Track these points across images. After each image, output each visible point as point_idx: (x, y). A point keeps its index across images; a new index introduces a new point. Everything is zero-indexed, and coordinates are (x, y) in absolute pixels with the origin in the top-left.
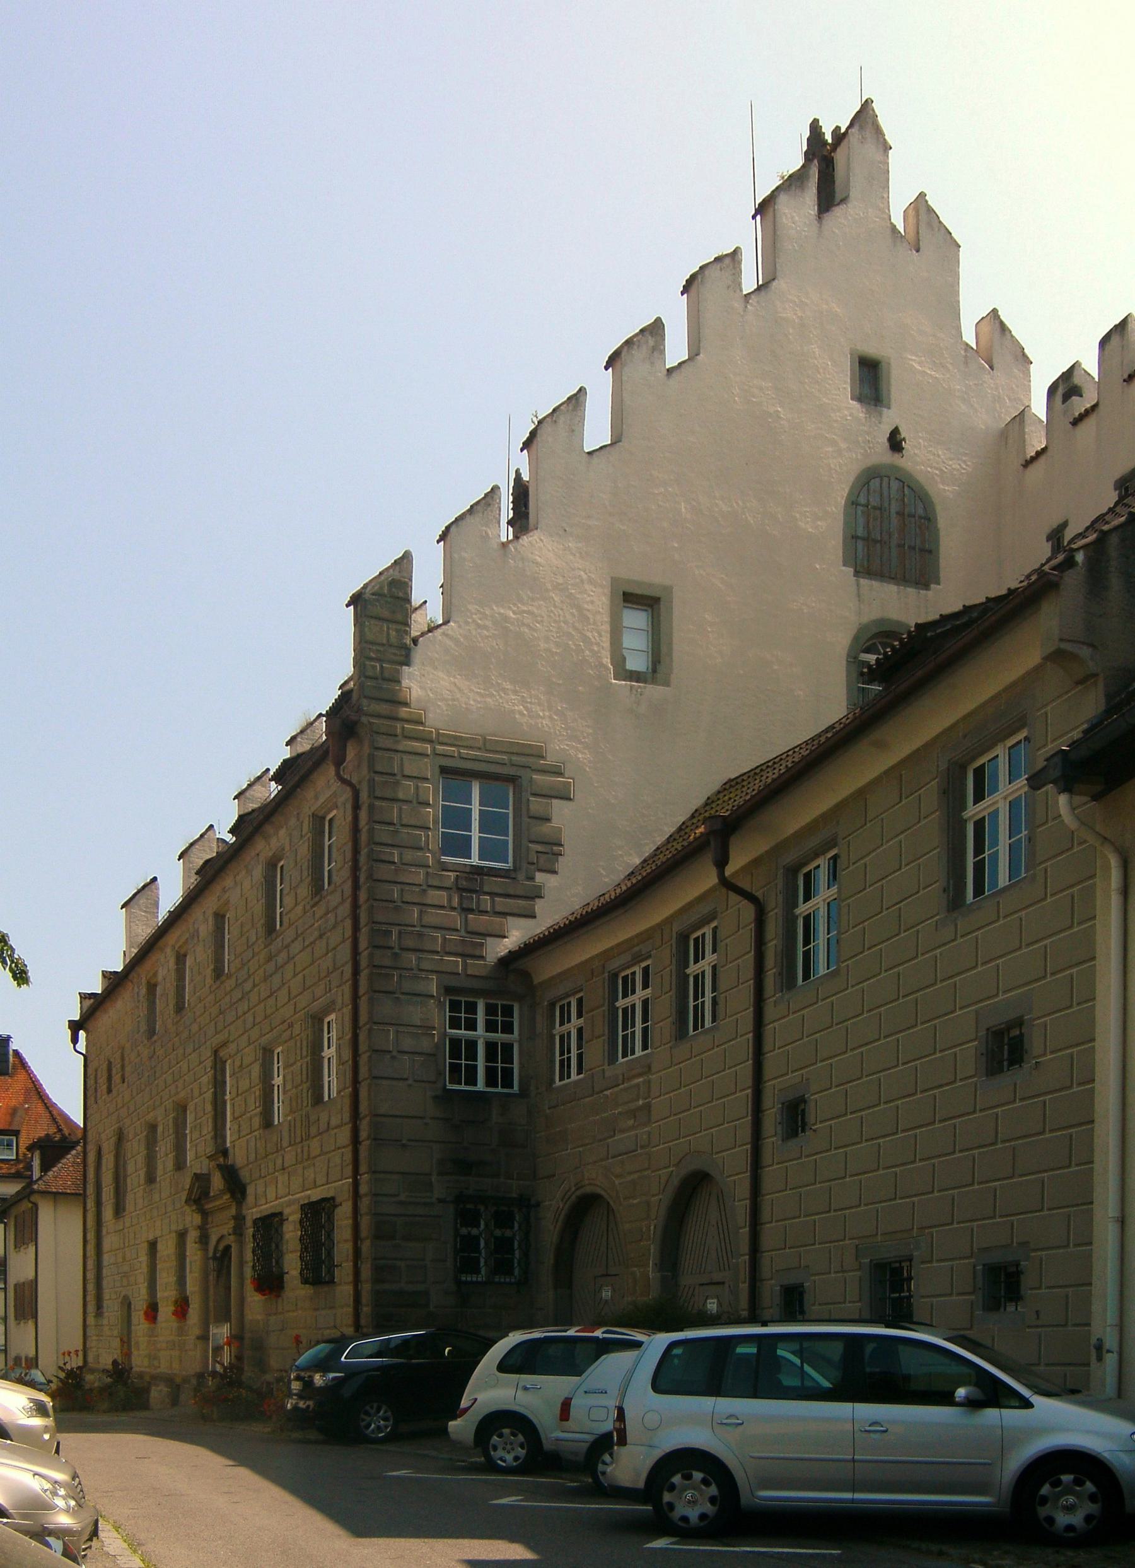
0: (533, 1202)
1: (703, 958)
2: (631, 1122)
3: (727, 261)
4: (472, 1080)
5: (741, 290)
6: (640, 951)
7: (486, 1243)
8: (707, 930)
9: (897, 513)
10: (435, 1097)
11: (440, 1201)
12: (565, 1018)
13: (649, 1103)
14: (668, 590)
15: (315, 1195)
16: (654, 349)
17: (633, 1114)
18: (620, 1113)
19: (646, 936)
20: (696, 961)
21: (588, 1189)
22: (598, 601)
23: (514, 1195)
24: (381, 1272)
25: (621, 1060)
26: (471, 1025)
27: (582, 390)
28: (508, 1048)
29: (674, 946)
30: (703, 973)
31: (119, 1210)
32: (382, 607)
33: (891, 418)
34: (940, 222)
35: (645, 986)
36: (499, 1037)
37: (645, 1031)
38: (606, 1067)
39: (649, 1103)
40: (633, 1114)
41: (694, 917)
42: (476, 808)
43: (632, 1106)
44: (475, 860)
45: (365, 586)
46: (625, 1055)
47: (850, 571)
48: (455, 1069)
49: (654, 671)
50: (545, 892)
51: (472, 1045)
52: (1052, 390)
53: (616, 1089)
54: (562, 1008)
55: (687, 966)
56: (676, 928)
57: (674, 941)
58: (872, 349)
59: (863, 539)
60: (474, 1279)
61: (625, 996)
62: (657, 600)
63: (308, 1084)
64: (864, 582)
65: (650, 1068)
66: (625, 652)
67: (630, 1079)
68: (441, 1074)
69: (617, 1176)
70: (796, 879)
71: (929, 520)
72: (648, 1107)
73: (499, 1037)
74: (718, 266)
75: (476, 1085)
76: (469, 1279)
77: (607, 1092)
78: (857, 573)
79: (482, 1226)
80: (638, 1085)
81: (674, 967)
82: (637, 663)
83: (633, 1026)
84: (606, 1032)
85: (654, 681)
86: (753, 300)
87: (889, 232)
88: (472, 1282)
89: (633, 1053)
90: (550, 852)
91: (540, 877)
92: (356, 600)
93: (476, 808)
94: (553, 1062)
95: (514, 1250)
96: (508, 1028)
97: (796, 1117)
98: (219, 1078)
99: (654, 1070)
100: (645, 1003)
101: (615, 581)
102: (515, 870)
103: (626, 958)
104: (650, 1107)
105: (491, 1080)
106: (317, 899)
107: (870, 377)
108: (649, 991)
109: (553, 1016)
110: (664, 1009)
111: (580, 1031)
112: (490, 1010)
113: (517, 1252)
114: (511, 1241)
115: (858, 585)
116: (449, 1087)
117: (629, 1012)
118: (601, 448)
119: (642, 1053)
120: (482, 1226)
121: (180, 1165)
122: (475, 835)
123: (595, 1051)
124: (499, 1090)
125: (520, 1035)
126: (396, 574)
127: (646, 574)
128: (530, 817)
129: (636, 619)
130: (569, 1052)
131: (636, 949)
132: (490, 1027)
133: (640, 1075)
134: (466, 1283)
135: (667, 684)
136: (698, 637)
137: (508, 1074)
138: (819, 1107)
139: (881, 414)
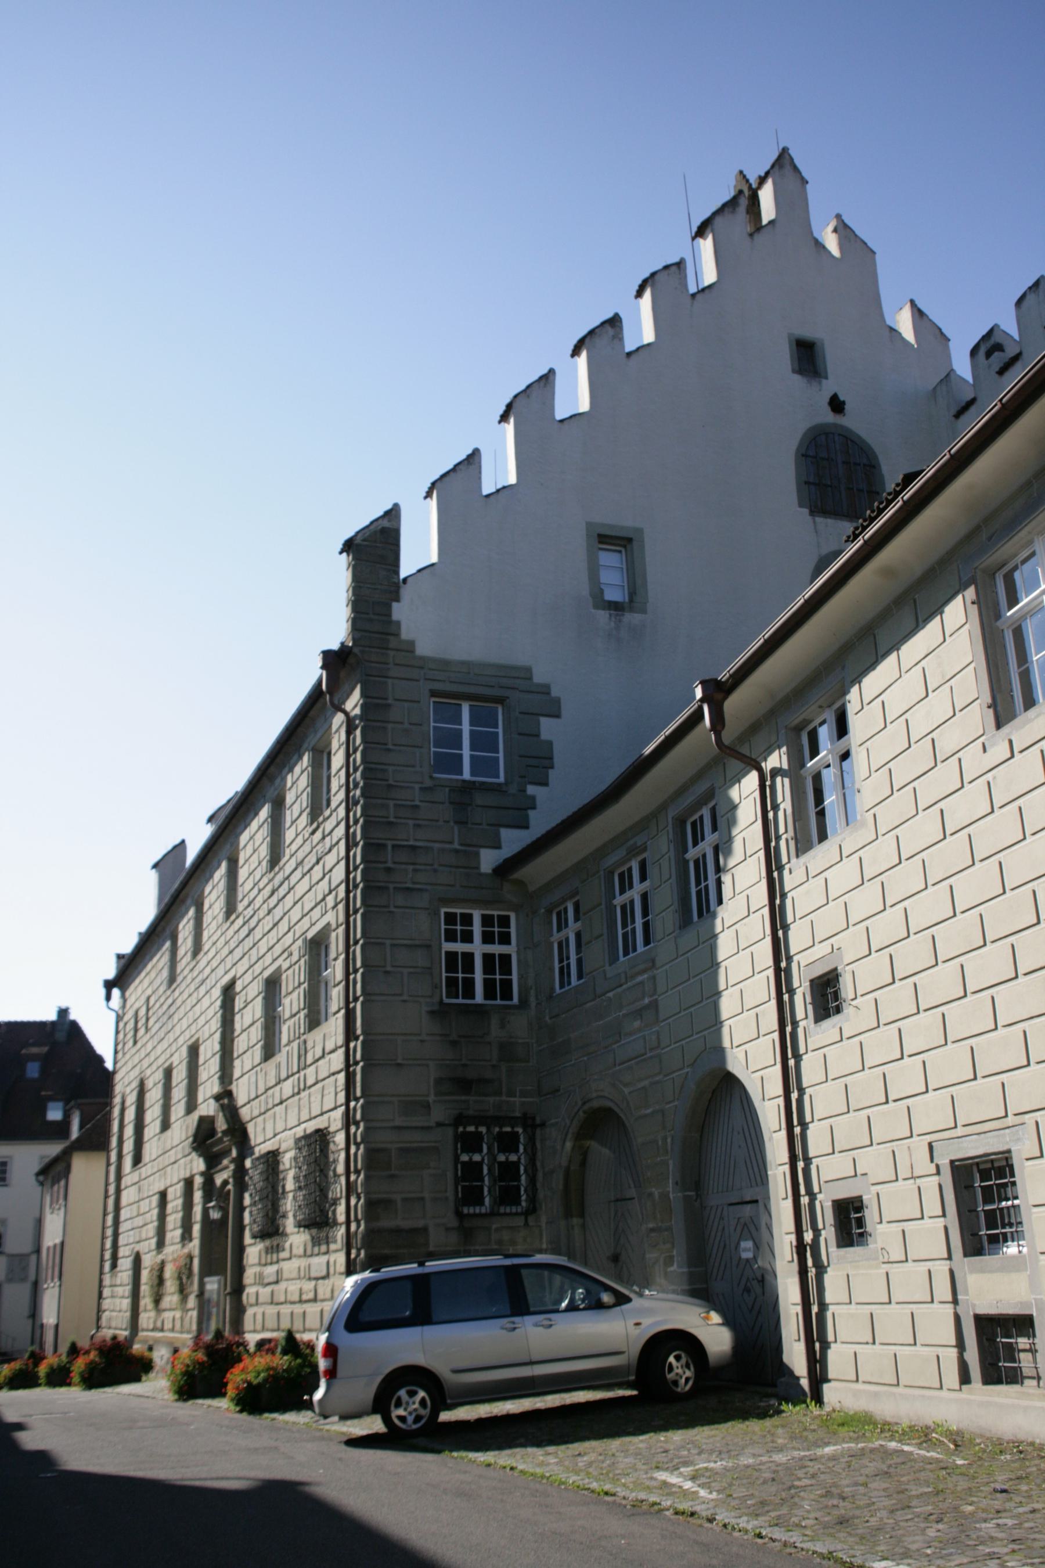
0: (538, 1121)
1: (703, 839)
2: (637, 1024)
3: (674, 268)
4: (469, 992)
5: (687, 290)
6: (635, 843)
7: (489, 1170)
8: (706, 812)
9: (843, 462)
10: (432, 1013)
11: (439, 1124)
12: (562, 924)
13: (656, 1000)
14: (640, 531)
15: (311, 1127)
16: (614, 337)
17: (639, 1013)
18: (625, 1016)
19: (642, 825)
20: (695, 843)
21: (596, 1104)
22: (578, 542)
23: (518, 1114)
24: (373, 1207)
25: (622, 959)
26: (468, 938)
27: (552, 371)
28: (506, 959)
29: (671, 831)
30: (704, 856)
31: (137, 1160)
32: (373, 550)
33: (829, 387)
34: (856, 235)
35: (643, 878)
36: (496, 949)
37: (646, 926)
38: (607, 968)
39: (656, 1000)
40: (639, 1013)
41: (689, 799)
42: (466, 727)
43: (639, 1005)
44: (467, 775)
45: (358, 533)
46: (626, 953)
47: (806, 511)
48: (452, 983)
49: (631, 601)
50: (539, 802)
51: (469, 957)
52: (974, 352)
53: (619, 990)
54: (559, 914)
55: (686, 851)
56: (672, 813)
57: (670, 828)
58: (807, 333)
59: (814, 484)
60: (477, 1211)
61: (622, 891)
62: (630, 540)
63: (306, 1011)
64: (819, 520)
65: (653, 961)
66: (602, 587)
67: (633, 977)
68: (437, 987)
69: (626, 1085)
70: (799, 737)
71: (874, 467)
72: (654, 1005)
73: (496, 949)
74: (666, 272)
75: (473, 998)
76: (471, 1211)
77: (610, 995)
78: (812, 513)
79: (485, 1150)
80: (642, 983)
81: (672, 854)
82: (613, 595)
83: (633, 921)
84: (605, 931)
85: (632, 610)
86: (698, 296)
87: (813, 243)
88: (475, 1215)
89: (635, 950)
90: (537, 763)
91: (531, 790)
92: (349, 546)
93: (466, 727)
94: (552, 969)
95: (520, 1176)
96: (505, 939)
97: (827, 995)
98: (228, 1018)
99: (658, 964)
100: (645, 897)
101: (589, 525)
102: (506, 783)
103: (621, 853)
104: (657, 1006)
105: (489, 994)
106: (315, 825)
107: (807, 356)
108: (647, 883)
109: (550, 923)
110: (665, 899)
111: (578, 935)
112: (487, 921)
113: (523, 1178)
114: (516, 1164)
115: (814, 522)
116: (446, 1000)
117: (627, 910)
118: (571, 417)
119: (643, 949)
120: (485, 1150)
121: (191, 1106)
122: (466, 752)
123: (596, 953)
124: (499, 1002)
125: (518, 945)
126: (386, 523)
127: (618, 517)
128: (520, 734)
129: (610, 560)
130: (568, 958)
131: (631, 842)
132: (487, 938)
133: (644, 971)
134: (469, 1215)
135: (644, 611)
136: (670, 569)
137: (507, 985)
138: (859, 980)
139: (820, 383)
